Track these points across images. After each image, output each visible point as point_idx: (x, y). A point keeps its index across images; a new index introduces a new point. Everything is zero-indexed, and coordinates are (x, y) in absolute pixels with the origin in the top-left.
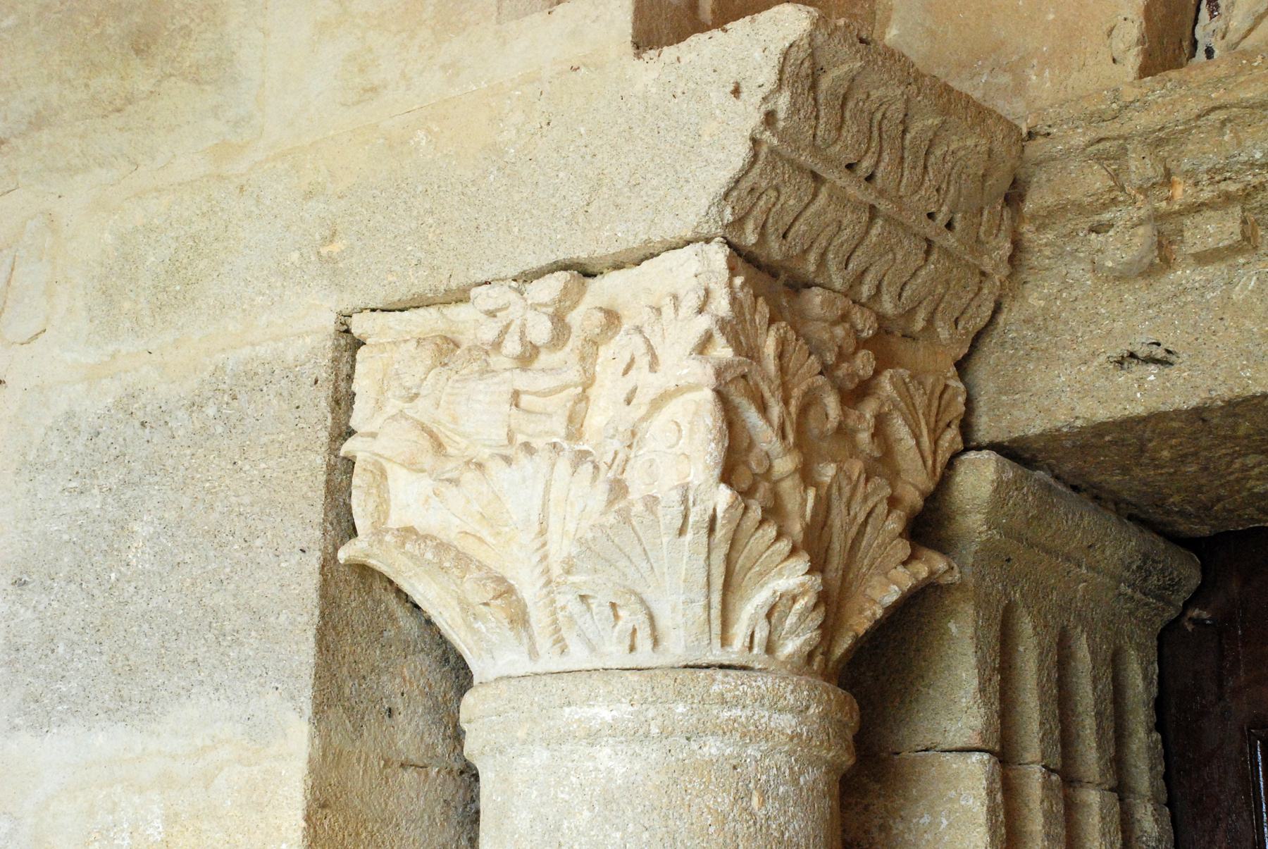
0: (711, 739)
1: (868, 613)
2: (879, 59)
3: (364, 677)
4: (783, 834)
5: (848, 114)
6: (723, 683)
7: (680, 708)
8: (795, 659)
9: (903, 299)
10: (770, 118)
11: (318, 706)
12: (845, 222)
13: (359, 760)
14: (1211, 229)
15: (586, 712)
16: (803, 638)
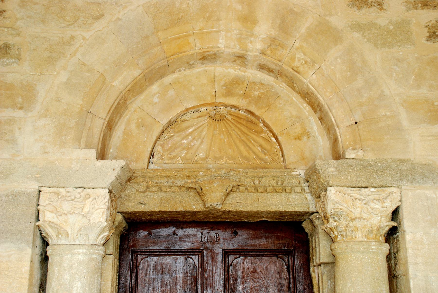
14: (154, 189)
15: (78, 250)
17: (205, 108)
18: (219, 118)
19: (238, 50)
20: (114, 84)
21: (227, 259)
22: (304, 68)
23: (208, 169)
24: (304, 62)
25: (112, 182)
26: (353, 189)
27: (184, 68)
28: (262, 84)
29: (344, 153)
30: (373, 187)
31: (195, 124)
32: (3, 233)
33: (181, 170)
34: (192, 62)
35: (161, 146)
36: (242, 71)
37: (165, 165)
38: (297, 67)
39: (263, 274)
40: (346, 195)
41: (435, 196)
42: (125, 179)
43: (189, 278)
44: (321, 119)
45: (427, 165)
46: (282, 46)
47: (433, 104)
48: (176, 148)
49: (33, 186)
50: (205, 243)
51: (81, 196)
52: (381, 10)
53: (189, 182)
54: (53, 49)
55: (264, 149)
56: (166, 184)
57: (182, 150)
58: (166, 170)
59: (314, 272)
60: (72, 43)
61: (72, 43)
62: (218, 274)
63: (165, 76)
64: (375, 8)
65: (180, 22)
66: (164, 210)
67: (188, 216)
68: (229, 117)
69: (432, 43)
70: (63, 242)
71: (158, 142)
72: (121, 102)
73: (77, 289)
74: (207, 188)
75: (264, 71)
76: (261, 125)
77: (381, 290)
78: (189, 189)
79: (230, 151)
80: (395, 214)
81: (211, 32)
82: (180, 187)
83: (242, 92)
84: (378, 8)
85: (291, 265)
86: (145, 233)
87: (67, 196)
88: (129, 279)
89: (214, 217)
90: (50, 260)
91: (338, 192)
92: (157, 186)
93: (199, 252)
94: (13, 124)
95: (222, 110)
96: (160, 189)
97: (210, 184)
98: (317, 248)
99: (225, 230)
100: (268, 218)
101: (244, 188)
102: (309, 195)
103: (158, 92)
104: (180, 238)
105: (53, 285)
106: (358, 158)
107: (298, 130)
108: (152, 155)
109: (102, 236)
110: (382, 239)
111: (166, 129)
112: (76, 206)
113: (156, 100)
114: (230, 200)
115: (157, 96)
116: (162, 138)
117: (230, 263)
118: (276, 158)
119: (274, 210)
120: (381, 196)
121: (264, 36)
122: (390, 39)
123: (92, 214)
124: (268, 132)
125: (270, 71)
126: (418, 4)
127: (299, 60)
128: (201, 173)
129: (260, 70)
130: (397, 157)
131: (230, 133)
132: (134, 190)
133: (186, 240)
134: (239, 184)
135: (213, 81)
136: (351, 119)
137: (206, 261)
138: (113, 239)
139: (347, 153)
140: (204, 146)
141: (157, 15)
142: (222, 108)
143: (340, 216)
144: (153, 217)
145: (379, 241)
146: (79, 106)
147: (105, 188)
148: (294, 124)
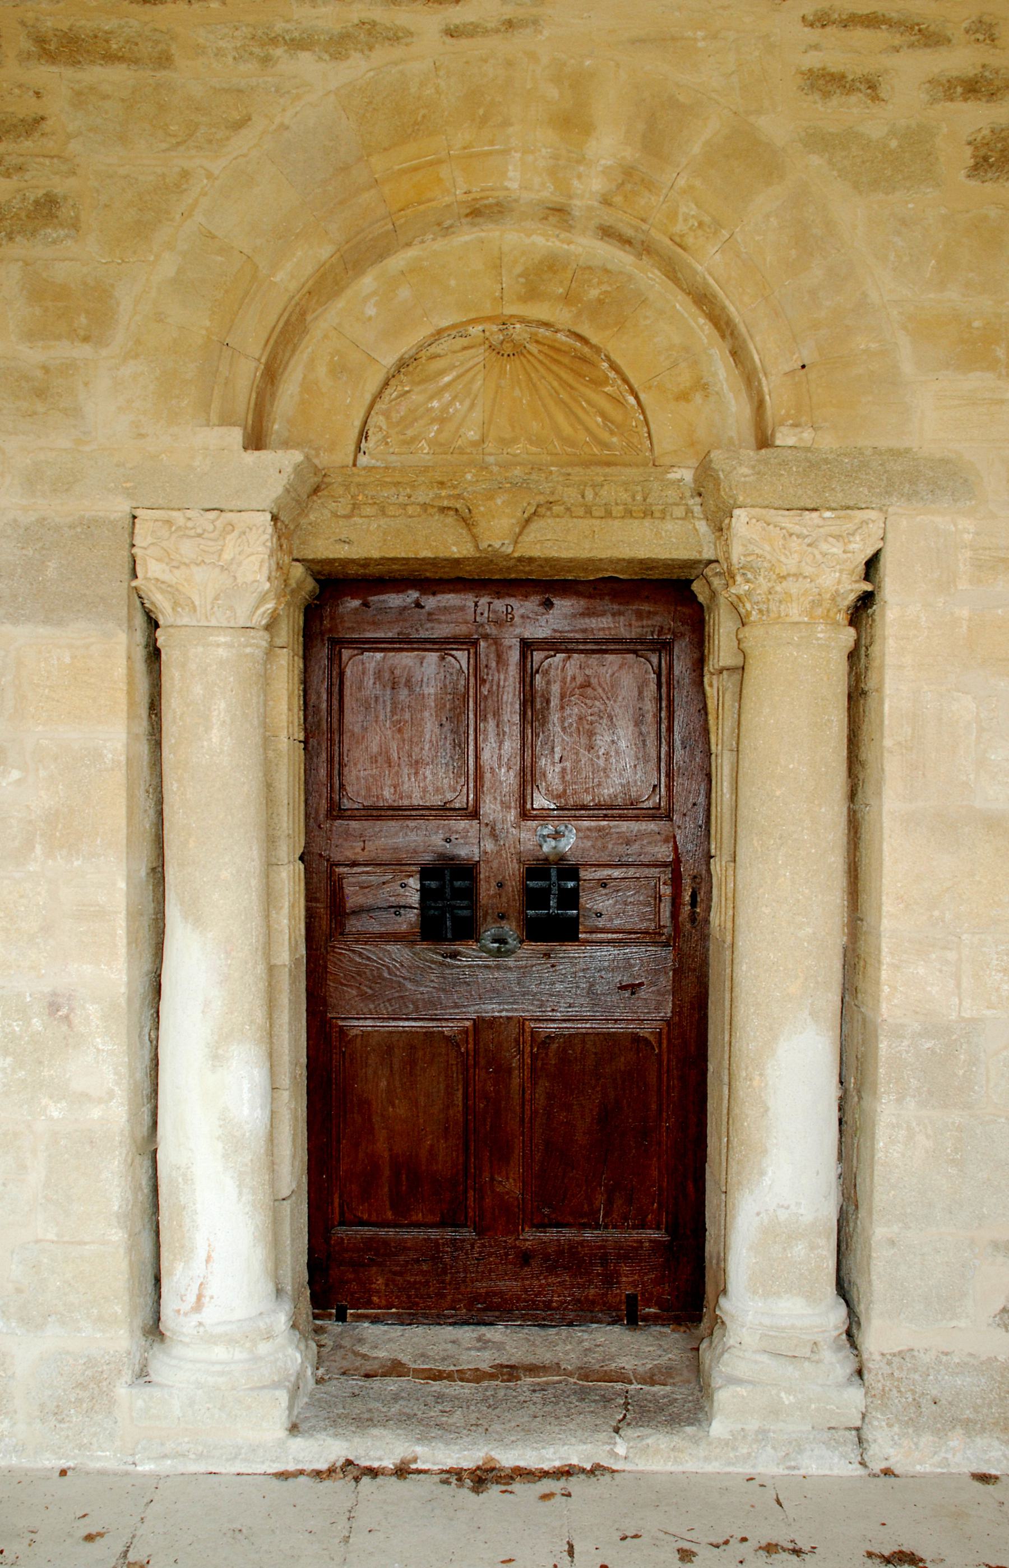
15: (217, 639)
17: (480, 328)
18: (509, 351)
19: (552, 193)
20: (277, 279)
21: (529, 660)
22: (696, 238)
23: (484, 467)
24: (696, 224)
25: (278, 498)
26: (787, 513)
27: (432, 236)
28: (606, 271)
29: (773, 435)
30: (830, 509)
31: (458, 363)
32: (71, 601)
33: (426, 469)
34: (448, 223)
35: (383, 414)
36: (563, 241)
37: (393, 458)
38: (682, 236)
39: (604, 689)
40: (771, 527)
41: (953, 529)
42: (304, 491)
43: (450, 697)
44: (734, 354)
45: (944, 461)
46: (649, 185)
47: (969, 325)
48: (416, 420)
49: (120, 507)
50: (482, 625)
51: (215, 527)
52: (873, 100)
53: (443, 494)
54: (146, 202)
55: (609, 421)
56: (394, 499)
57: (429, 424)
58: (394, 469)
59: (711, 685)
60: (184, 186)
61: (184, 186)
62: (511, 689)
63: (389, 255)
64: (861, 95)
65: (418, 130)
66: (392, 555)
67: (444, 567)
68: (533, 348)
69: (978, 183)
70: (185, 621)
71: (377, 407)
72: (293, 319)
73: (219, 713)
74: (482, 509)
75: (611, 240)
76: (606, 365)
77: (828, 720)
78: (443, 510)
79: (535, 426)
80: (872, 566)
81: (490, 153)
82: (424, 506)
83: (561, 290)
84: (867, 95)
85: (664, 672)
86: (356, 603)
87: (186, 528)
88: (325, 697)
89: (501, 570)
90: (163, 657)
91: (754, 521)
92: (375, 503)
93: (469, 643)
94: (73, 375)
95: (517, 331)
96: (383, 512)
97: (488, 499)
98: (716, 637)
99: (526, 596)
100: (616, 572)
101: (562, 508)
102: (704, 523)
103: (374, 293)
104: (430, 614)
105: (173, 705)
106: (802, 445)
107: (685, 379)
108: (363, 435)
109: (262, 610)
110: (842, 618)
111: (394, 376)
112: (207, 549)
113: (371, 311)
114: (533, 535)
115: (373, 300)
116: (386, 396)
117: (535, 667)
118: (635, 441)
119: (626, 557)
120: (844, 528)
121: (609, 163)
122: (888, 172)
123: (240, 564)
124: (619, 382)
125: (626, 242)
126: (955, 88)
127: (685, 220)
128: (469, 477)
129: (602, 239)
130: (883, 444)
131: (534, 385)
132: (326, 512)
133: (443, 618)
134: (551, 500)
135: (497, 265)
136: (795, 357)
137: (485, 663)
138: (288, 616)
139: (778, 435)
140: (477, 415)
141: (368, 115)
142: (518, 326)
143: (756, 572)
144: (371, 570)
145: (836, 624)
146: (204, 332)
147: (263, 511)
148: (675, 365)
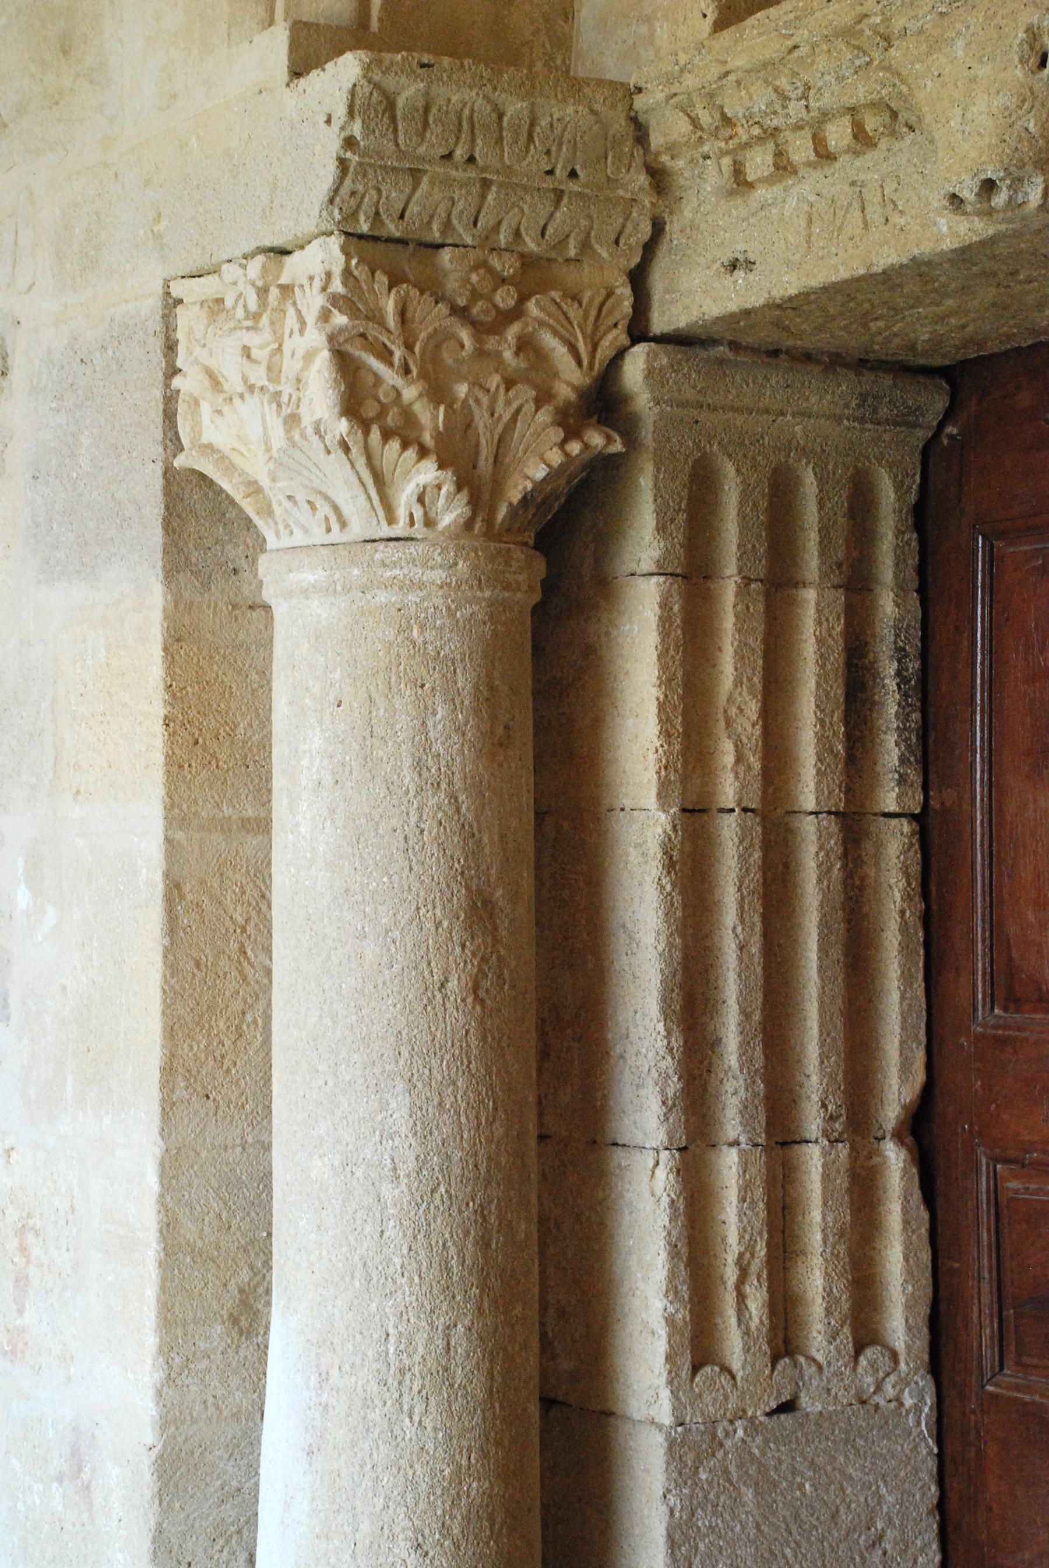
0: (378, 592)
1: (520, 488)
2: (444, 75)
3: (209, 549)
4: (439, 653)
5: (431, 119)
6: (383, 552)
7: (356, 572)
8: (452, 528)
9: (547, 237)
10: (349, 143)
11: (168, 572)
12: (456, 197)
13: (209, 607)
16: (455, 514)
